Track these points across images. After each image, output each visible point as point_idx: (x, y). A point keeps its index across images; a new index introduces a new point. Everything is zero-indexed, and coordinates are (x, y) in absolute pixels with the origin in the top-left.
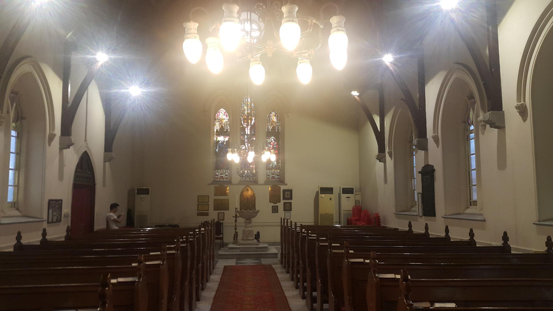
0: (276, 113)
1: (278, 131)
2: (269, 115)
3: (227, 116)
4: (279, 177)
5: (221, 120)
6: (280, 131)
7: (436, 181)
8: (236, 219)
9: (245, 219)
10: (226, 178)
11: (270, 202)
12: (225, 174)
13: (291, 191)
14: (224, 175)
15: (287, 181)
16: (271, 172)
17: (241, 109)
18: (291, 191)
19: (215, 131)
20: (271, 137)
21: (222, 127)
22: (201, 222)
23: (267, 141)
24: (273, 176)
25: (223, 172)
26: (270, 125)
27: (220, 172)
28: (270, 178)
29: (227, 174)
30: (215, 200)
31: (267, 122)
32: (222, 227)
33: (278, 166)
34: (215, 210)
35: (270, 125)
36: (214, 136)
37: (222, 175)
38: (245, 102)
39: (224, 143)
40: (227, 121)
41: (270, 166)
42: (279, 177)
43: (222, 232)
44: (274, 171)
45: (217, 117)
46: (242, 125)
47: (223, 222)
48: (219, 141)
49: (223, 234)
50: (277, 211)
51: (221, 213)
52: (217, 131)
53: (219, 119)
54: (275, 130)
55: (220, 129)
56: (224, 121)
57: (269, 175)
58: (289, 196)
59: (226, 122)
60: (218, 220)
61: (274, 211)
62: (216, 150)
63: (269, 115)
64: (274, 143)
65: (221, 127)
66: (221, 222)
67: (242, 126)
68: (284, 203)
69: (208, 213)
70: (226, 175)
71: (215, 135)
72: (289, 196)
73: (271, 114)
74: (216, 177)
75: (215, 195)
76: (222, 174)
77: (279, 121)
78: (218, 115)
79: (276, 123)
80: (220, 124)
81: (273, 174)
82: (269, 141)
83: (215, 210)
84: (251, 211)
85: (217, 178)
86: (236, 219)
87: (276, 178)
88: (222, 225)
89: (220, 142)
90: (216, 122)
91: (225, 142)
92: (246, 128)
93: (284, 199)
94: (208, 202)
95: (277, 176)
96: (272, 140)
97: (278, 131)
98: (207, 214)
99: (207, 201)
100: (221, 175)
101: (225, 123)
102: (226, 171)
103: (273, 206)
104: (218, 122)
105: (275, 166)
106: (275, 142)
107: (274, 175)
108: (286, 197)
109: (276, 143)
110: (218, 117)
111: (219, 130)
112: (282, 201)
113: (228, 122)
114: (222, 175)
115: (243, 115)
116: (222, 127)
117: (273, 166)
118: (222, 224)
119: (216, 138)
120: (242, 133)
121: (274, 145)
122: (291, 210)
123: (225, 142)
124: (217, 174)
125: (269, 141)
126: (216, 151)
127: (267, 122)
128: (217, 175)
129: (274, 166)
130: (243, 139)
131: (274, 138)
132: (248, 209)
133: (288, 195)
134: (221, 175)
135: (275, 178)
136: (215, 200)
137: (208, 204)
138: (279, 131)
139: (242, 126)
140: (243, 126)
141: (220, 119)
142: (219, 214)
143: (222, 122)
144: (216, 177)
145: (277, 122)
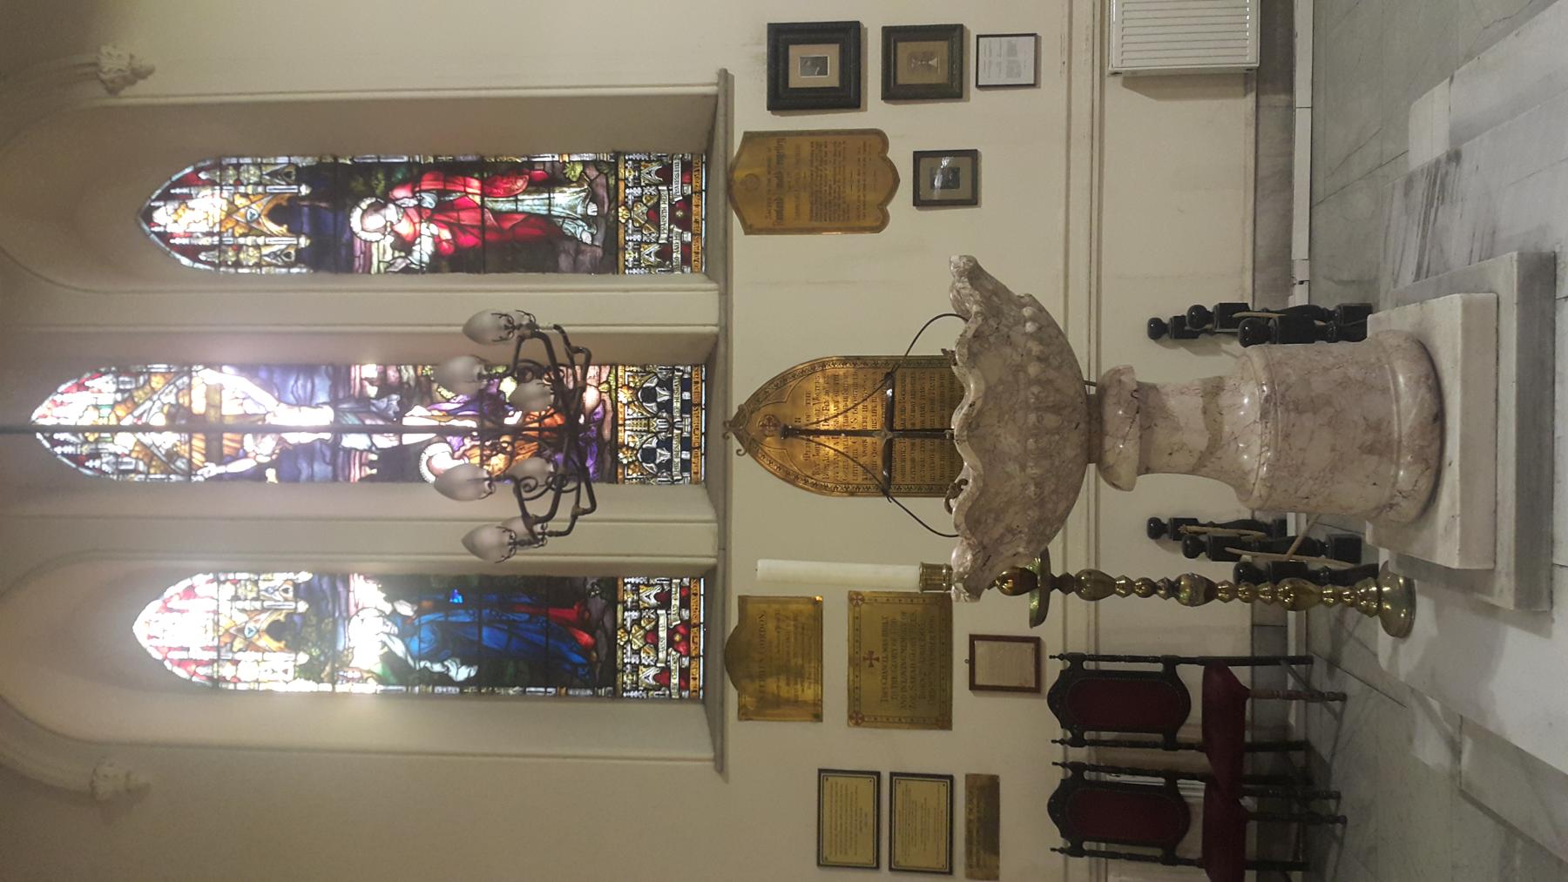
0: (166, 197)
1: (302, 175)
2: (184, 250)
3: (190, 592)
4: (677, 171)
5: (228, 642)
6: (304, 156)
7: (920, 210)
8: (1067, 584)
9: (1092, 467)
10: (685, 603)
11: (878, 229)
12: (656, 608)
13: (782, 37)
14: (662, 621)
15: (697, 79)
16: (639, 230)
17: (137, 478)
18: (782, 37)
19: (309, 686)
20: (353, 234)
21: (275, 630)
22: (1059, 857)
23: (390, 264)
24: (673, 220)
25: (636, 622)
26: (257, 247)
27: (637, 652)
28: (688, 237)
29: (649, 596)
30: (857, 717)
31: (238, 264)
32: (1105, 666)
33: (592, 173)
34: (943, 721)
35: (257, 247)
36: (347, 695)
37: (663, 634)
38: (85, 449)
39: (405, 618)
40: (228, 590)
41: (586, 238)
42: (677, 171)
43: (1159, 667)
44: (630, 210)
45: (202, 671)
46: (258, 474)
47: (1061, 657)
48: (389, 658)
49: (1171, 662)
50: (968, 160)
51: (972, 661)
52: (307, 672)
53: (214, 655)
54: (296, 198)
55: (294, 646)
56: (232, 616)
57: (665, 253)
58: (831, 53)
59: (236, 598)
60: (1036, 690)
61: (964, 192)
62: (462, 685)
63: (184, 250)
64: (405, 211)
65: (278, 639)
66: (1053, 671)
67: (271, 474)
68: (894, 92)
69: (971, 779)
70: (664, 601)
71: (340, 688)
72: (831, 53)
73: (172, 236)
74: (675, 680)
75: (818, 717)
76: (651, 637)
77: (223, 169)
78: (181, 663)
79: (246, 195)
80: (250, 646)
81: (653, 214)
82: (383, 250)
83: (943, 721)
84: (972, 390)
85: (685, 674)
86: (1067, 584)
87: (688, 190)
88: (1089, 665)
89: (399, 648)
90: (236, 680)
91: (394, 611)
92: (281, 441)
93: (847, 97)
94: (878, 774)
95: (668, 181)
96: (375, 221)
97: (302, 175)
98: (986, 791)
99: (866, 786)
100: (663, 644)
101: (244, 611)
102: (629, 598)
103: (919, 202)
104: (236, 663)
105: (592, 197)
106: (394, 201)
107: (664, 206)
108: (831, 79)
109: (399, 193)
110: (199, 663)
111: (303, 658)
112: (876, 113)
113: (235, 582)
114: (663, 634)
115: (179, 463)
116: (275, 630)
117: (585, 218)
118: (1076, 659)
119: (363, 680)
120: (321, 469)
121: (419, 208)
122: (952, 34)
123: (394, 611)
124: (652, 672)
125: (383, 250)
126: (468, 681)
127: (238, 264)
128: (663, 676)
129: (592, 209)
130: (371, 464)
131: (365, 212)
132: (940, 433)
133: (820, 65)
134: (663, 644)
135: (687, 200)
136: (857, 717)
137: (892, 775)
138: (308, 168)
139: (271, 474)
140: (269, 465)
141: (218, 649)
142: (979, 681)
143: (241, 630)
144: (675, 680)
145: (238, 183)
